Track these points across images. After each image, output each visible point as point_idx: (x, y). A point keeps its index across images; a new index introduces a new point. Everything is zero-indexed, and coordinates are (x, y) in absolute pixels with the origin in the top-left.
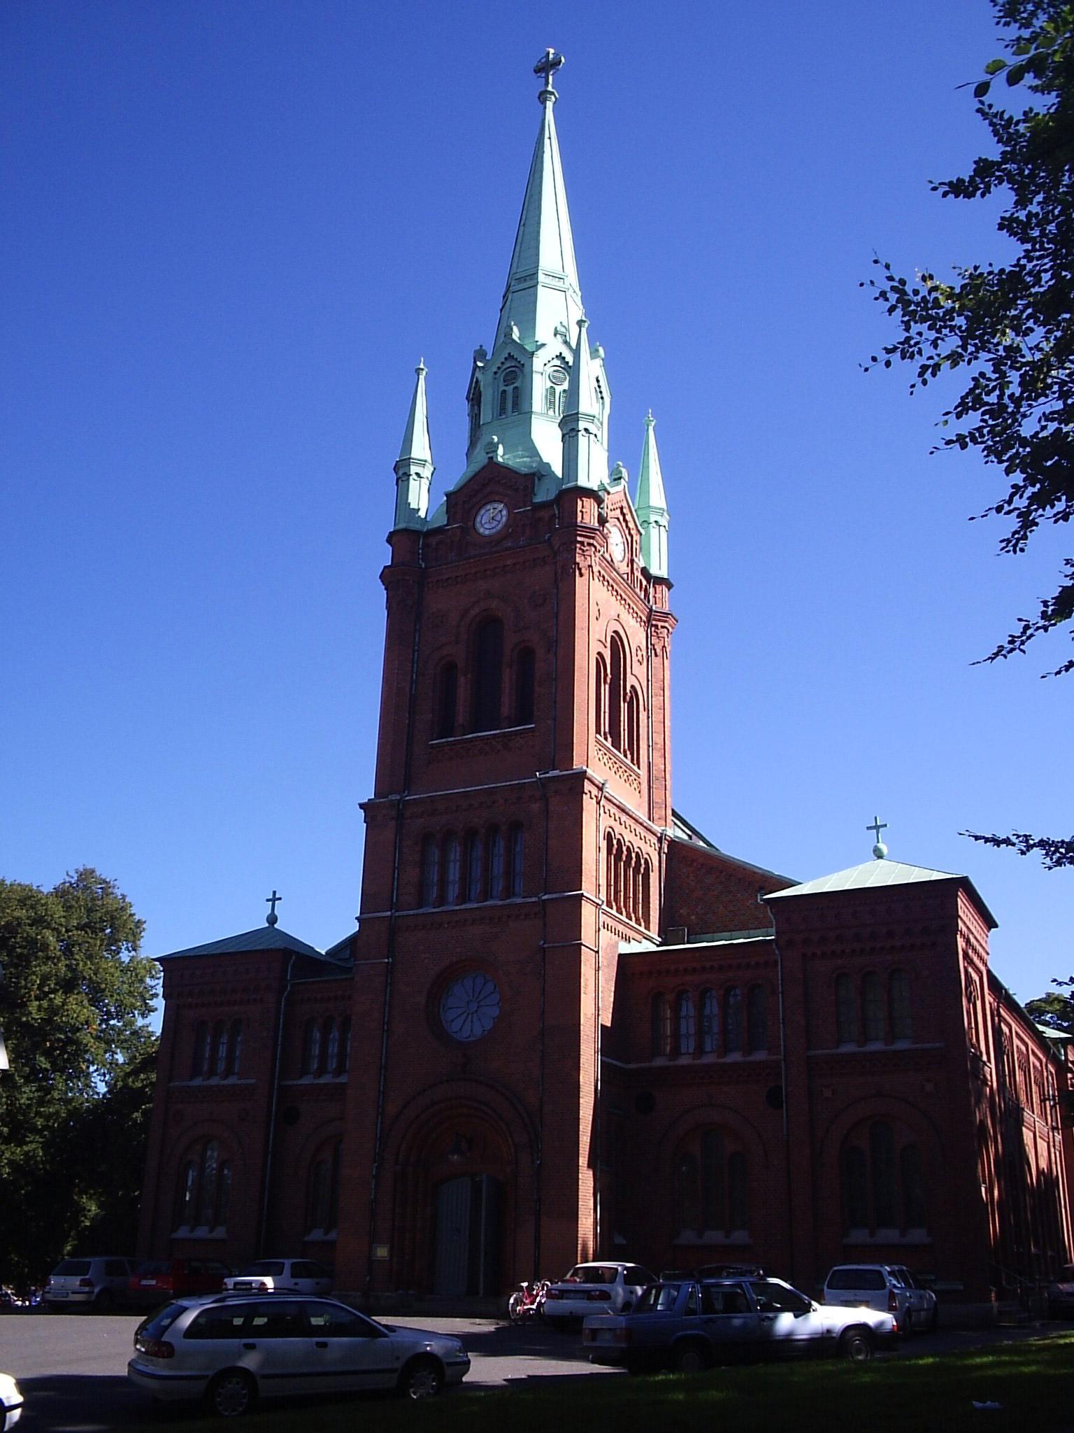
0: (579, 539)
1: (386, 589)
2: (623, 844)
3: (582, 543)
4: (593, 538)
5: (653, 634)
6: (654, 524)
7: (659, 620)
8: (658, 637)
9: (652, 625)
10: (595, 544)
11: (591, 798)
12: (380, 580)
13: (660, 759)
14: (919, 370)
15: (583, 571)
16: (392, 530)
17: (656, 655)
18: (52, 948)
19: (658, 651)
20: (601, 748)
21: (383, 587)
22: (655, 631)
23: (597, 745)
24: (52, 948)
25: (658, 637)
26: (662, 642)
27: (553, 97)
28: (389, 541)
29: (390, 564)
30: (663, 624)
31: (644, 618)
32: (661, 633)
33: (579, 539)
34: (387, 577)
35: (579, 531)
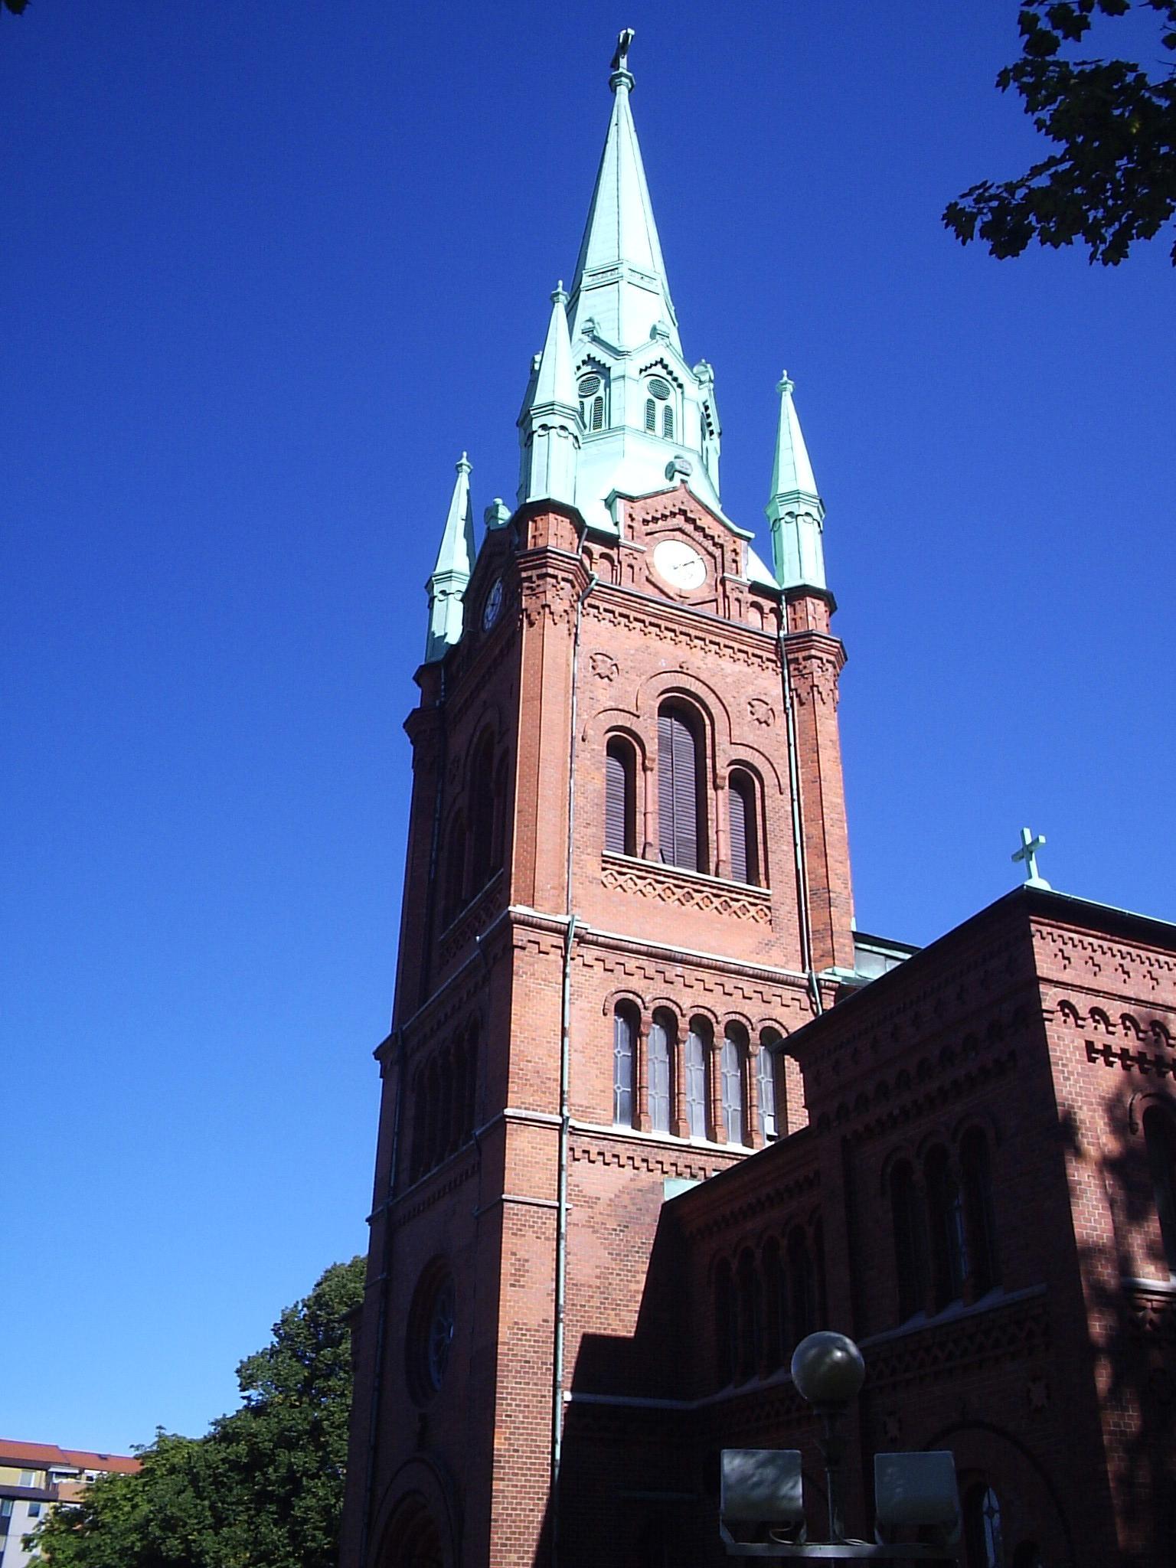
0: (524, 575)
1: (412, 742)
2: (714, 1020)
3: (529, 579)
4: (545, 565)
5: (793, 673)
6: (788, 518)
7: (799, 650)
8: (803, 675)
9: (789, 662)
10: (551, 571)
11: (1161, 967)
12: (404, 730)
13: (819, 860)
14: (998, 79)
15: (534, 616)
16: (423, 663)
17: (802, 704)
18: (328, 1289)
19: (804, 695)
20: (624, 870)
21: (409, 740)
22: (795, 669)
23: (608, 866)
24: (328, 1289)
25: (803, 675)
26: (810, 680)
27: (623, 79)
28: (417, 678)
29: (419, 706)
30: (806, 653)
31: (773, 657)
32: (805, 667)
33: (524, 575)
34: (414, 725)
35: (521, 563)
